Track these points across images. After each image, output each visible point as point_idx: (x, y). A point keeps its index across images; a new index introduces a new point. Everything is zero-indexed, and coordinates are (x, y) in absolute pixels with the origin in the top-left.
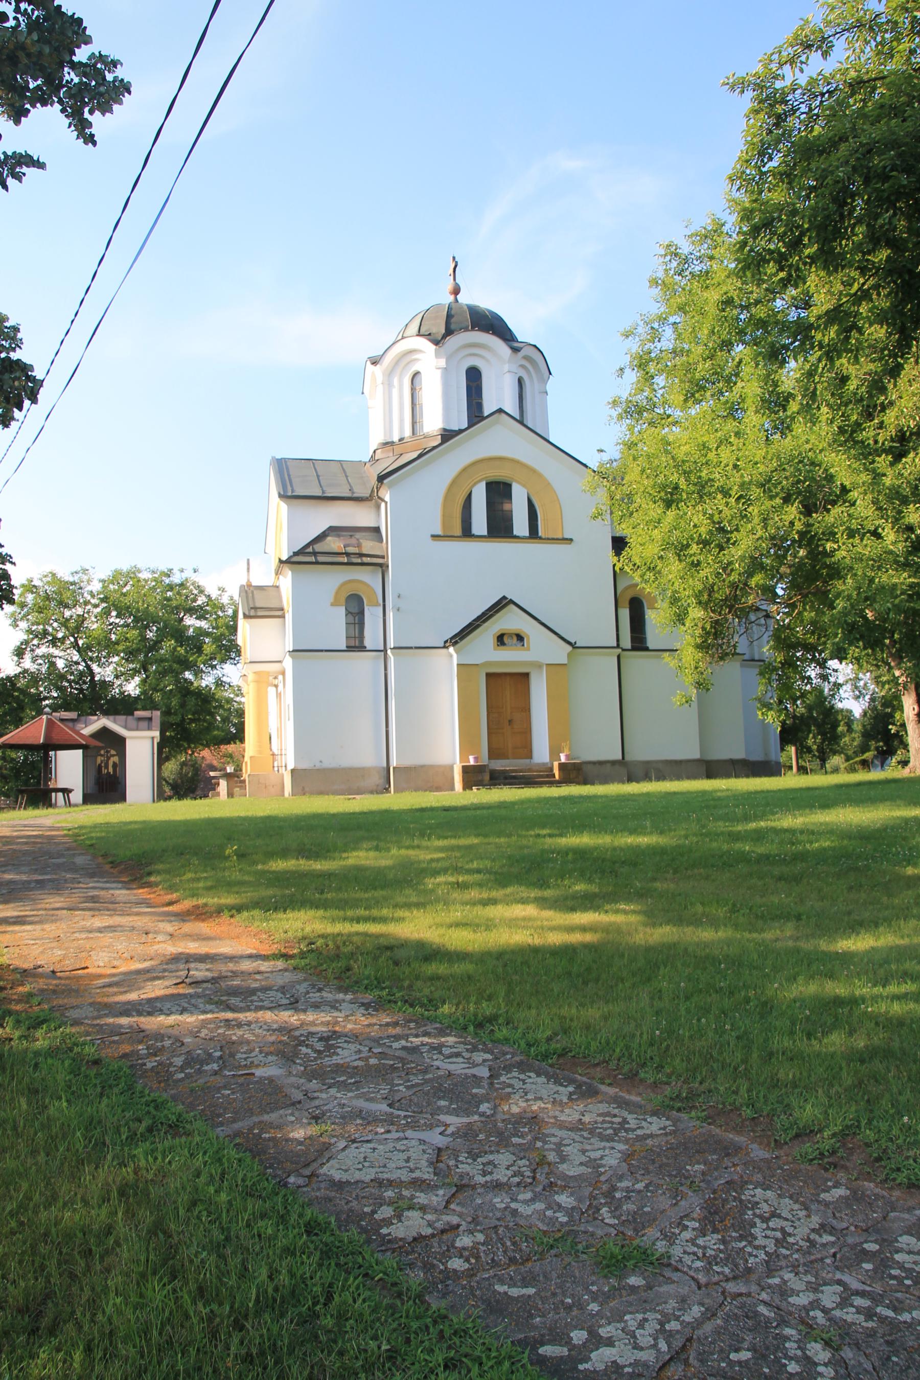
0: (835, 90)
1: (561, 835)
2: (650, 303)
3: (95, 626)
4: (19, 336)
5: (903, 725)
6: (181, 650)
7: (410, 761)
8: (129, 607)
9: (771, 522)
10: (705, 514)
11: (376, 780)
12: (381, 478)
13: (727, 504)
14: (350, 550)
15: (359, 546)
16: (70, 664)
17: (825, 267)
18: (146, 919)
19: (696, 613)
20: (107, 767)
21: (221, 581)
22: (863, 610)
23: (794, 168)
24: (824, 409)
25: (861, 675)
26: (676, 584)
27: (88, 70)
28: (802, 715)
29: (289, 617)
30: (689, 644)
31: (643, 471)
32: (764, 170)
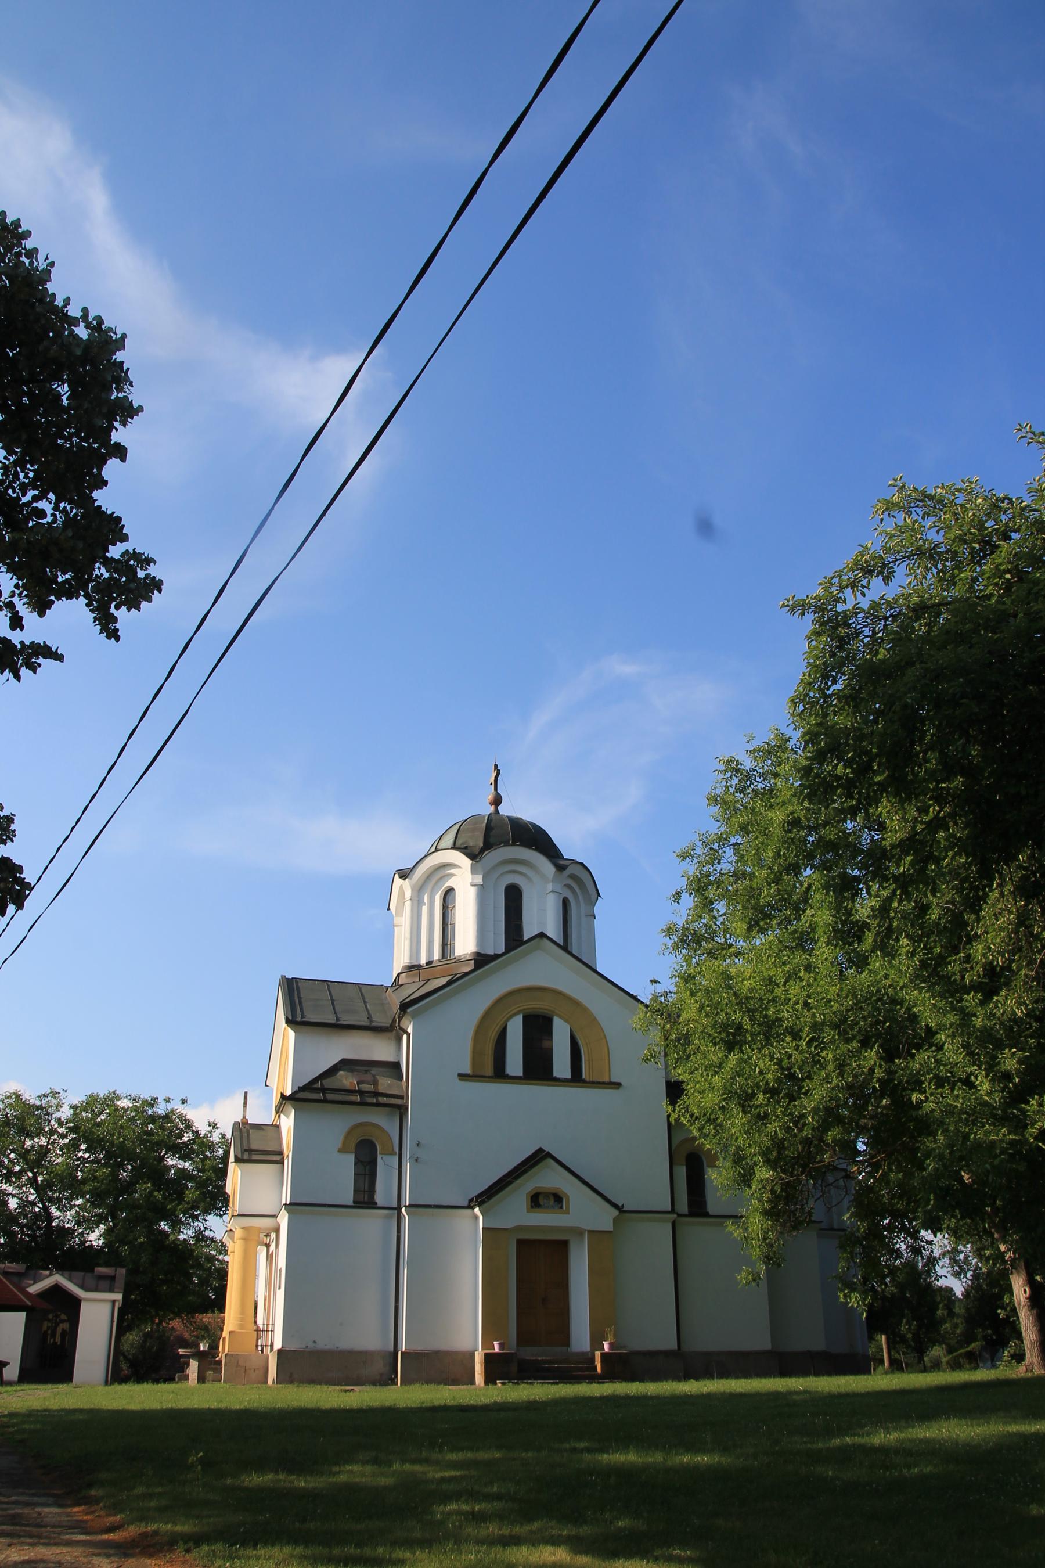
0: (899, 614)
1: (603, 1450)
2: (709, 822)
3: (59, 1160)
4: (13, 827)
5: (1014, 1310)
6: (158, 1196)
7: (419, 1347)
8: (102, 1140)
9: (848, 1069)
10: (772, 1058)
11: (379, 1367)
12: (404, 1007)
13: (797, 1048)
14: (365, 1087)
15: (375, 1083)
16: (24, 1204)
17: (897, 794)
18: (77, 1551)
19: (763, 1173)
20: (54, 1335)
21: (214, 1115)
22: (958, 1172)
23: (859, 691)
24: (904, 941)
25: (960, 1247)
26: (740, 1140)
27: (120, 566)
28: (893, 1294)
29: (288, 1163)
30: (756, 1210)
31: (702, 1008)
32: (829, 692)
